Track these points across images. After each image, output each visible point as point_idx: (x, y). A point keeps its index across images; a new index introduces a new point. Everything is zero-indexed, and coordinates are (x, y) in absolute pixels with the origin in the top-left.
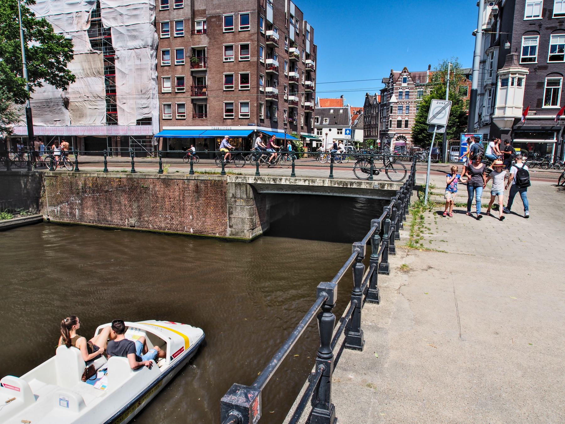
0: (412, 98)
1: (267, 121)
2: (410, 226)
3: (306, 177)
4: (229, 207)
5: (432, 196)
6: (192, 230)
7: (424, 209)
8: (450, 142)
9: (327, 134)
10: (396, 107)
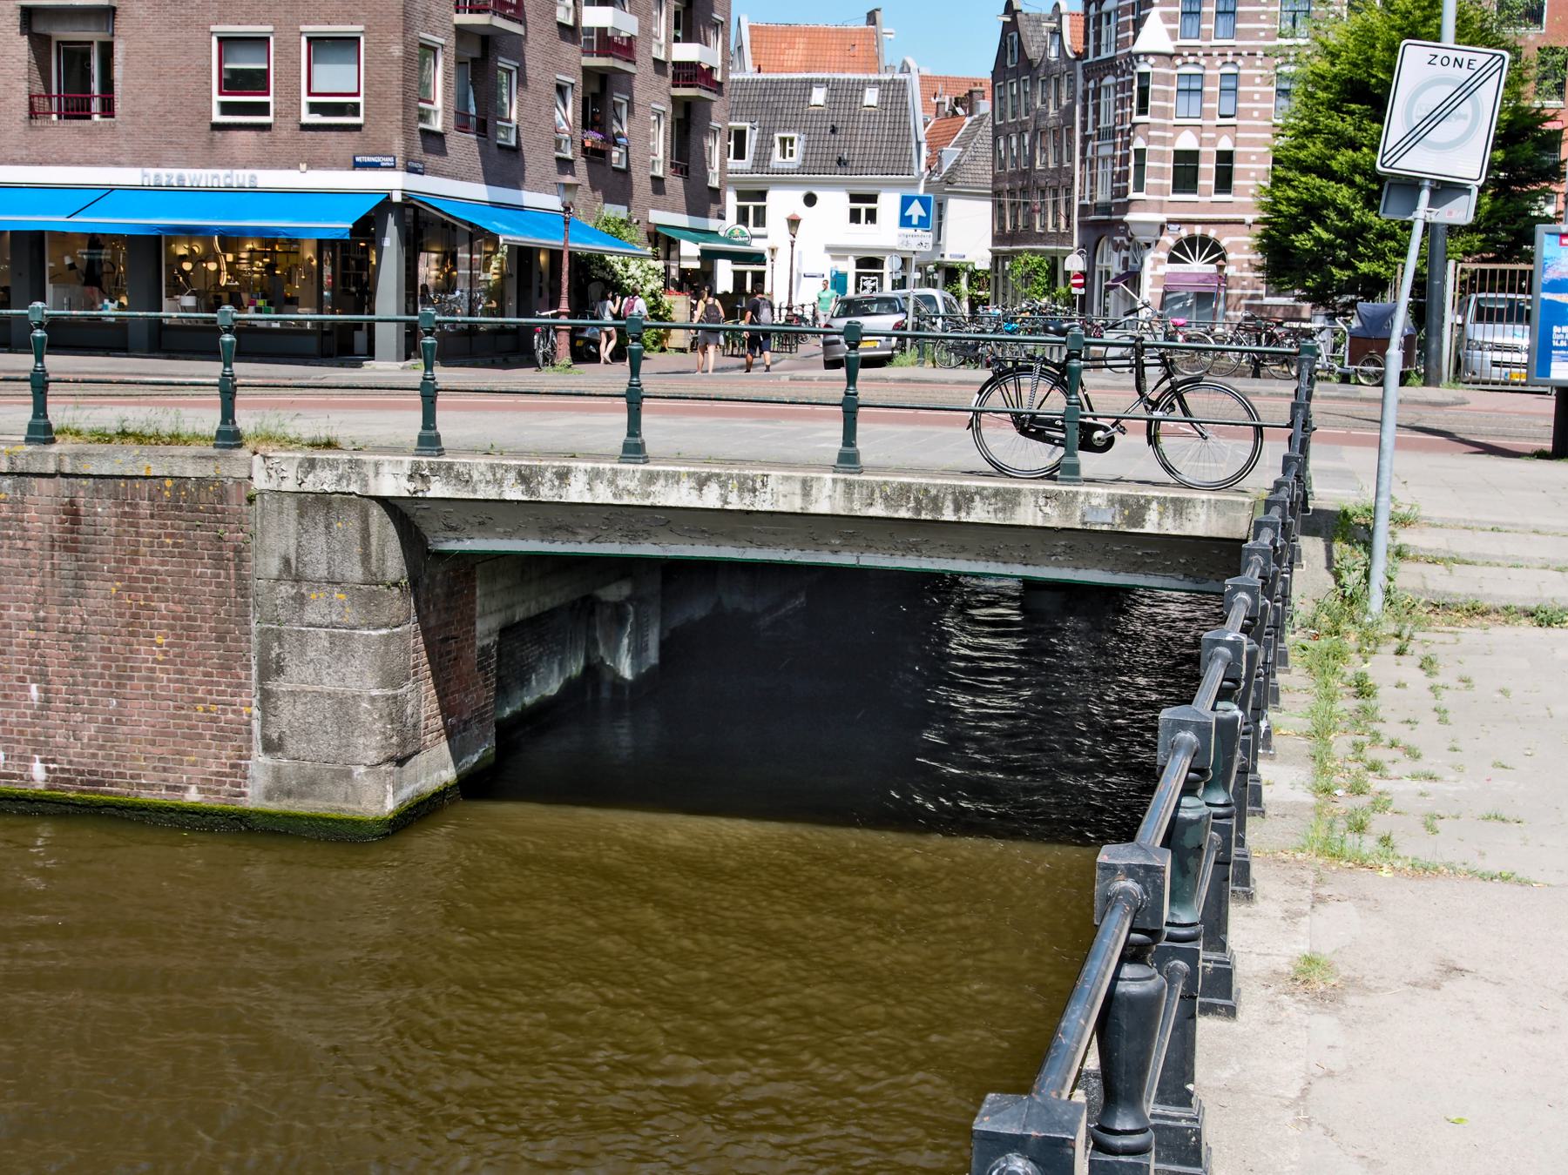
0: (1252, 34)
1: (463, 146)
2: (1308, 736)
3: (708, 461)
4: (263, 633)
5: (1404, 566)
6: (38, 771)
7: (1370, 642)
8: (1463, 271)
9: (794, 223)
10: (1167, 79)
